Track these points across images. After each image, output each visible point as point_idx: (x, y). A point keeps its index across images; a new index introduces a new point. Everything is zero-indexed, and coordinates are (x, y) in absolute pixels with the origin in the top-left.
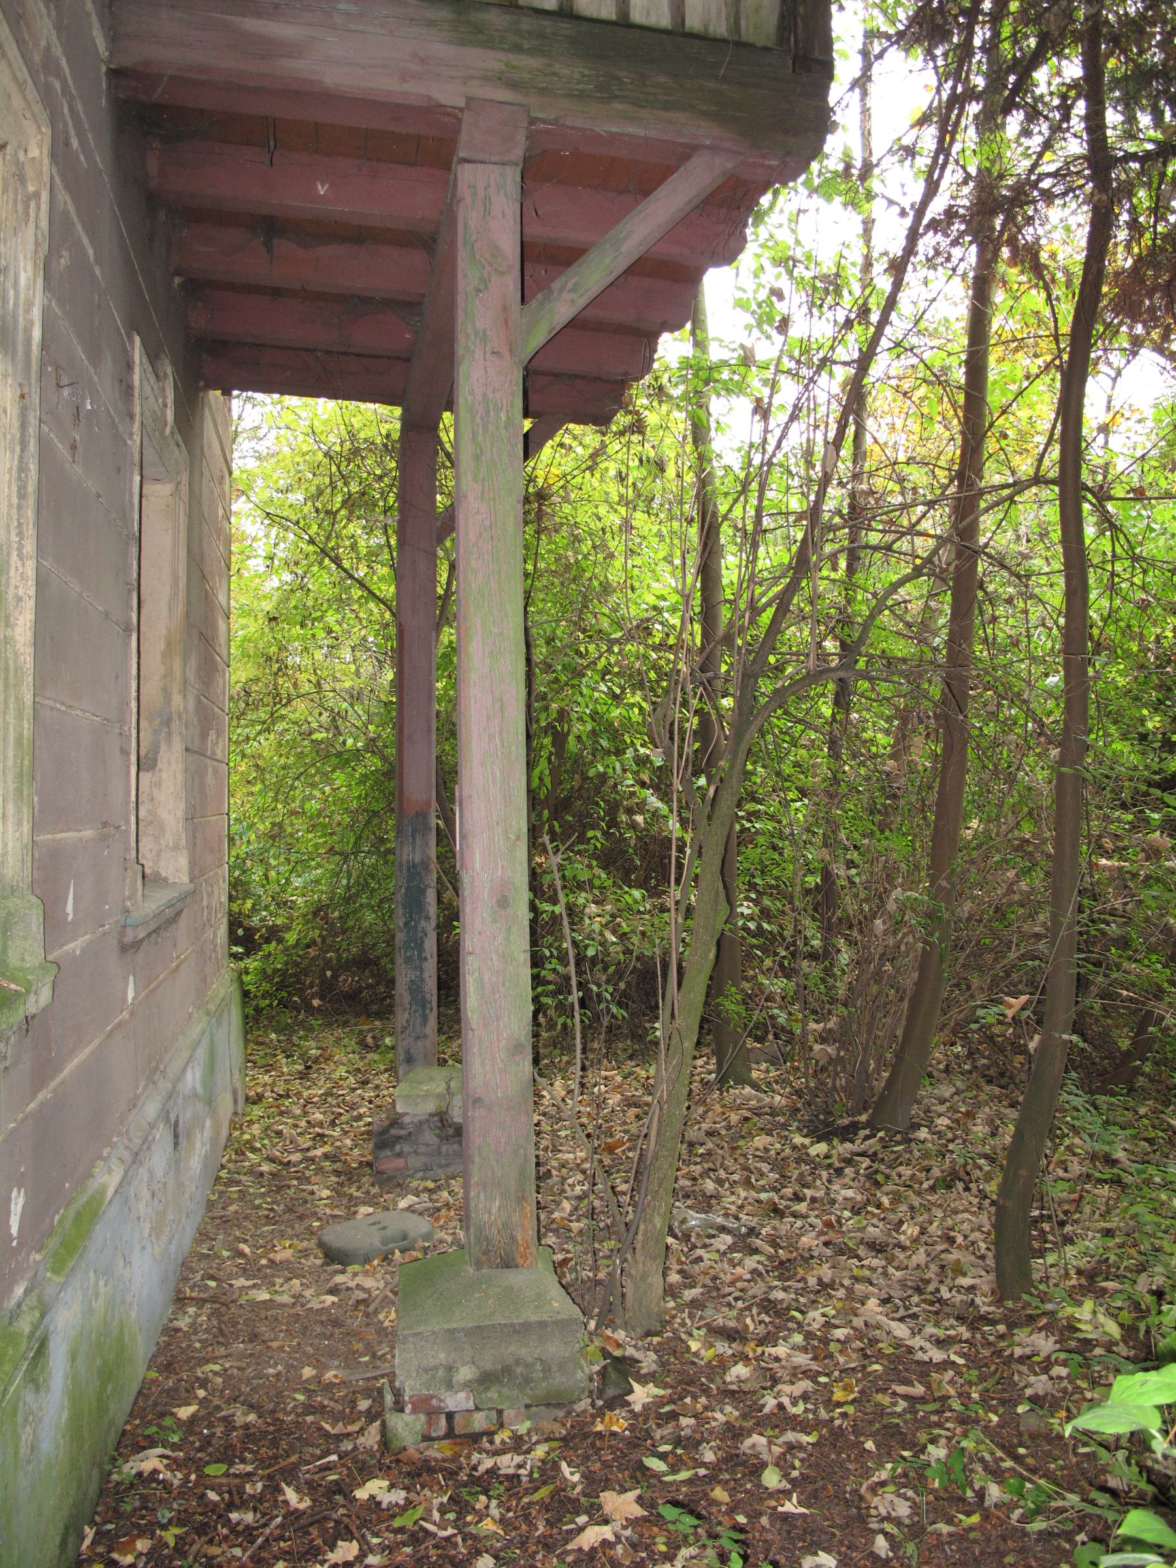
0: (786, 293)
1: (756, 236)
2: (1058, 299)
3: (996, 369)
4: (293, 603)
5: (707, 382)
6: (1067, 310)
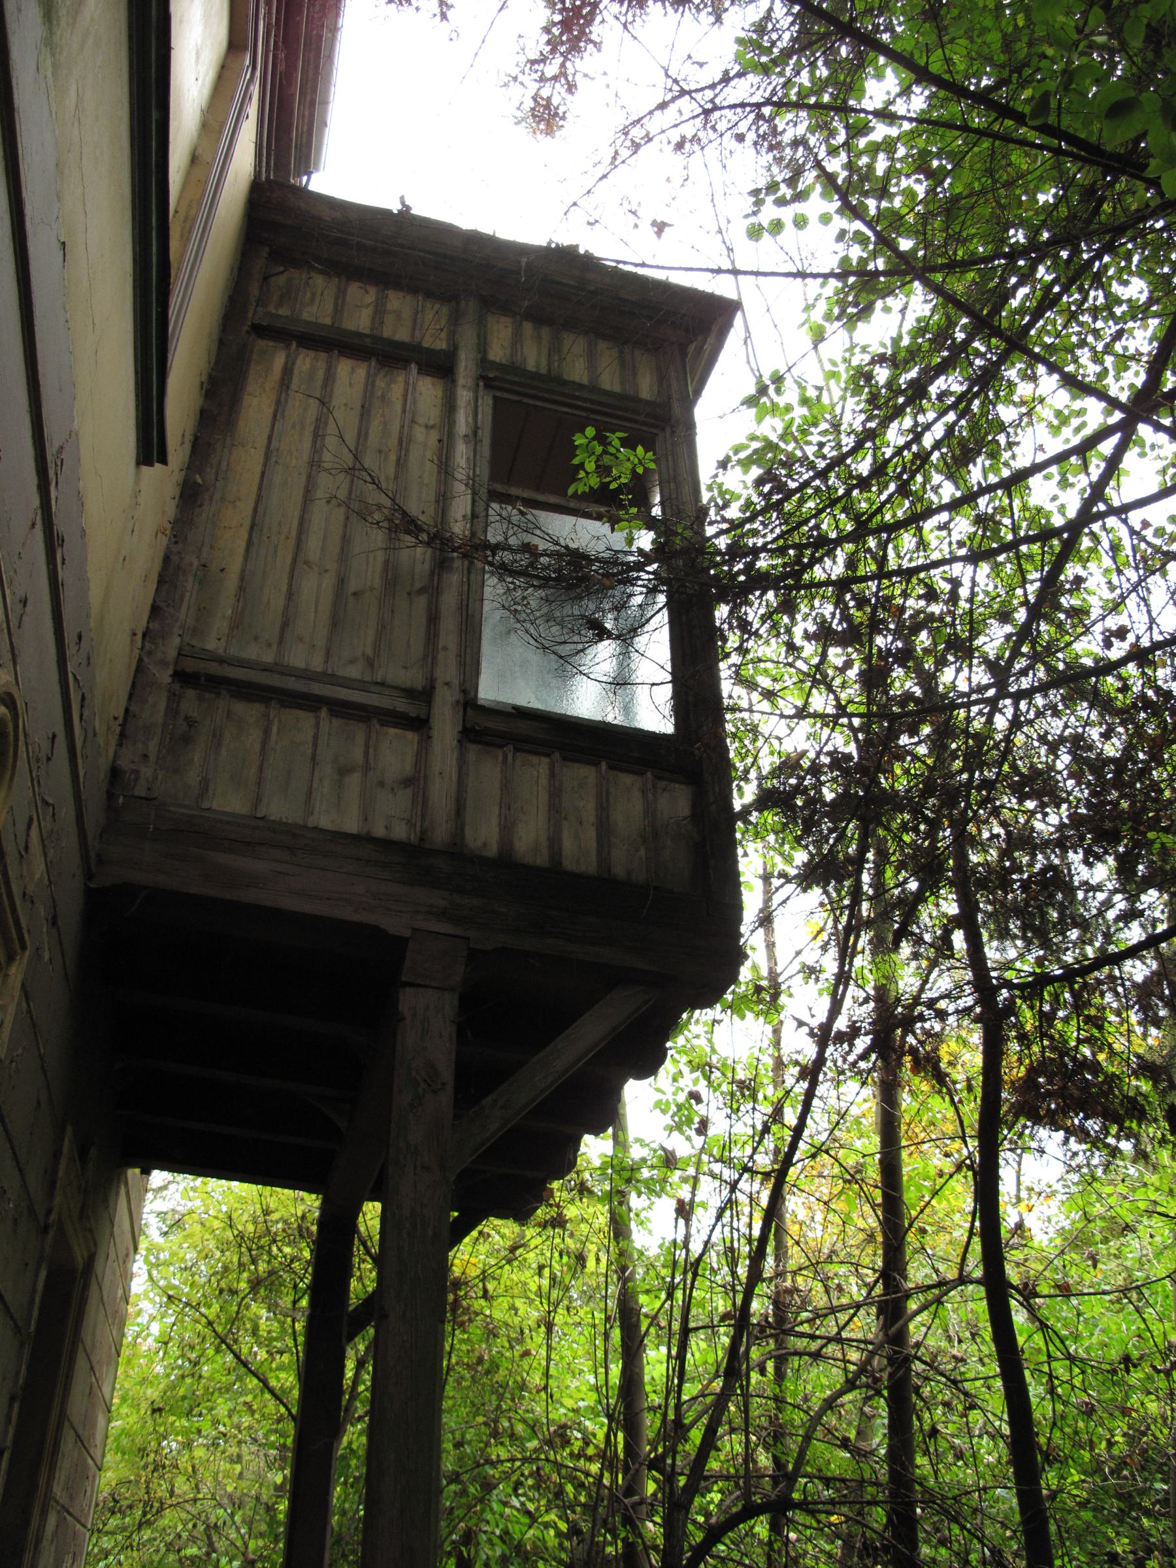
0: (704, 1097)
1: (676, 1044)
2: (961, 1101)
3: (910, 1164)
4: (182, 1392)
5: (629, 1181)
6: (971, 1111)
